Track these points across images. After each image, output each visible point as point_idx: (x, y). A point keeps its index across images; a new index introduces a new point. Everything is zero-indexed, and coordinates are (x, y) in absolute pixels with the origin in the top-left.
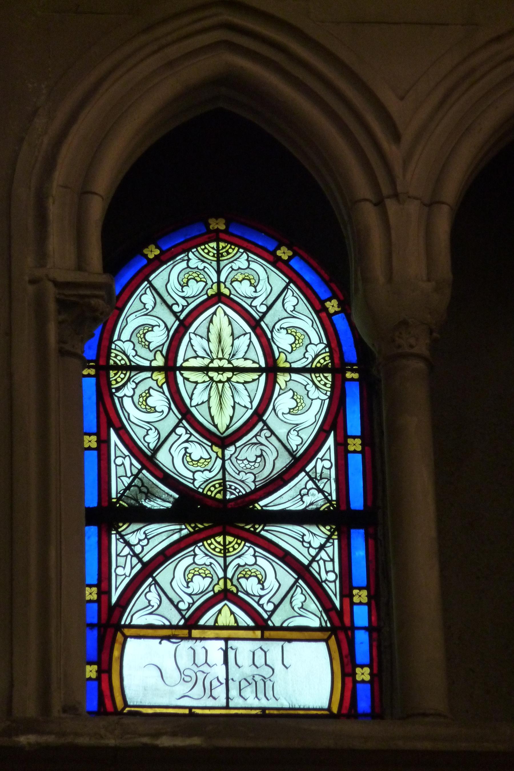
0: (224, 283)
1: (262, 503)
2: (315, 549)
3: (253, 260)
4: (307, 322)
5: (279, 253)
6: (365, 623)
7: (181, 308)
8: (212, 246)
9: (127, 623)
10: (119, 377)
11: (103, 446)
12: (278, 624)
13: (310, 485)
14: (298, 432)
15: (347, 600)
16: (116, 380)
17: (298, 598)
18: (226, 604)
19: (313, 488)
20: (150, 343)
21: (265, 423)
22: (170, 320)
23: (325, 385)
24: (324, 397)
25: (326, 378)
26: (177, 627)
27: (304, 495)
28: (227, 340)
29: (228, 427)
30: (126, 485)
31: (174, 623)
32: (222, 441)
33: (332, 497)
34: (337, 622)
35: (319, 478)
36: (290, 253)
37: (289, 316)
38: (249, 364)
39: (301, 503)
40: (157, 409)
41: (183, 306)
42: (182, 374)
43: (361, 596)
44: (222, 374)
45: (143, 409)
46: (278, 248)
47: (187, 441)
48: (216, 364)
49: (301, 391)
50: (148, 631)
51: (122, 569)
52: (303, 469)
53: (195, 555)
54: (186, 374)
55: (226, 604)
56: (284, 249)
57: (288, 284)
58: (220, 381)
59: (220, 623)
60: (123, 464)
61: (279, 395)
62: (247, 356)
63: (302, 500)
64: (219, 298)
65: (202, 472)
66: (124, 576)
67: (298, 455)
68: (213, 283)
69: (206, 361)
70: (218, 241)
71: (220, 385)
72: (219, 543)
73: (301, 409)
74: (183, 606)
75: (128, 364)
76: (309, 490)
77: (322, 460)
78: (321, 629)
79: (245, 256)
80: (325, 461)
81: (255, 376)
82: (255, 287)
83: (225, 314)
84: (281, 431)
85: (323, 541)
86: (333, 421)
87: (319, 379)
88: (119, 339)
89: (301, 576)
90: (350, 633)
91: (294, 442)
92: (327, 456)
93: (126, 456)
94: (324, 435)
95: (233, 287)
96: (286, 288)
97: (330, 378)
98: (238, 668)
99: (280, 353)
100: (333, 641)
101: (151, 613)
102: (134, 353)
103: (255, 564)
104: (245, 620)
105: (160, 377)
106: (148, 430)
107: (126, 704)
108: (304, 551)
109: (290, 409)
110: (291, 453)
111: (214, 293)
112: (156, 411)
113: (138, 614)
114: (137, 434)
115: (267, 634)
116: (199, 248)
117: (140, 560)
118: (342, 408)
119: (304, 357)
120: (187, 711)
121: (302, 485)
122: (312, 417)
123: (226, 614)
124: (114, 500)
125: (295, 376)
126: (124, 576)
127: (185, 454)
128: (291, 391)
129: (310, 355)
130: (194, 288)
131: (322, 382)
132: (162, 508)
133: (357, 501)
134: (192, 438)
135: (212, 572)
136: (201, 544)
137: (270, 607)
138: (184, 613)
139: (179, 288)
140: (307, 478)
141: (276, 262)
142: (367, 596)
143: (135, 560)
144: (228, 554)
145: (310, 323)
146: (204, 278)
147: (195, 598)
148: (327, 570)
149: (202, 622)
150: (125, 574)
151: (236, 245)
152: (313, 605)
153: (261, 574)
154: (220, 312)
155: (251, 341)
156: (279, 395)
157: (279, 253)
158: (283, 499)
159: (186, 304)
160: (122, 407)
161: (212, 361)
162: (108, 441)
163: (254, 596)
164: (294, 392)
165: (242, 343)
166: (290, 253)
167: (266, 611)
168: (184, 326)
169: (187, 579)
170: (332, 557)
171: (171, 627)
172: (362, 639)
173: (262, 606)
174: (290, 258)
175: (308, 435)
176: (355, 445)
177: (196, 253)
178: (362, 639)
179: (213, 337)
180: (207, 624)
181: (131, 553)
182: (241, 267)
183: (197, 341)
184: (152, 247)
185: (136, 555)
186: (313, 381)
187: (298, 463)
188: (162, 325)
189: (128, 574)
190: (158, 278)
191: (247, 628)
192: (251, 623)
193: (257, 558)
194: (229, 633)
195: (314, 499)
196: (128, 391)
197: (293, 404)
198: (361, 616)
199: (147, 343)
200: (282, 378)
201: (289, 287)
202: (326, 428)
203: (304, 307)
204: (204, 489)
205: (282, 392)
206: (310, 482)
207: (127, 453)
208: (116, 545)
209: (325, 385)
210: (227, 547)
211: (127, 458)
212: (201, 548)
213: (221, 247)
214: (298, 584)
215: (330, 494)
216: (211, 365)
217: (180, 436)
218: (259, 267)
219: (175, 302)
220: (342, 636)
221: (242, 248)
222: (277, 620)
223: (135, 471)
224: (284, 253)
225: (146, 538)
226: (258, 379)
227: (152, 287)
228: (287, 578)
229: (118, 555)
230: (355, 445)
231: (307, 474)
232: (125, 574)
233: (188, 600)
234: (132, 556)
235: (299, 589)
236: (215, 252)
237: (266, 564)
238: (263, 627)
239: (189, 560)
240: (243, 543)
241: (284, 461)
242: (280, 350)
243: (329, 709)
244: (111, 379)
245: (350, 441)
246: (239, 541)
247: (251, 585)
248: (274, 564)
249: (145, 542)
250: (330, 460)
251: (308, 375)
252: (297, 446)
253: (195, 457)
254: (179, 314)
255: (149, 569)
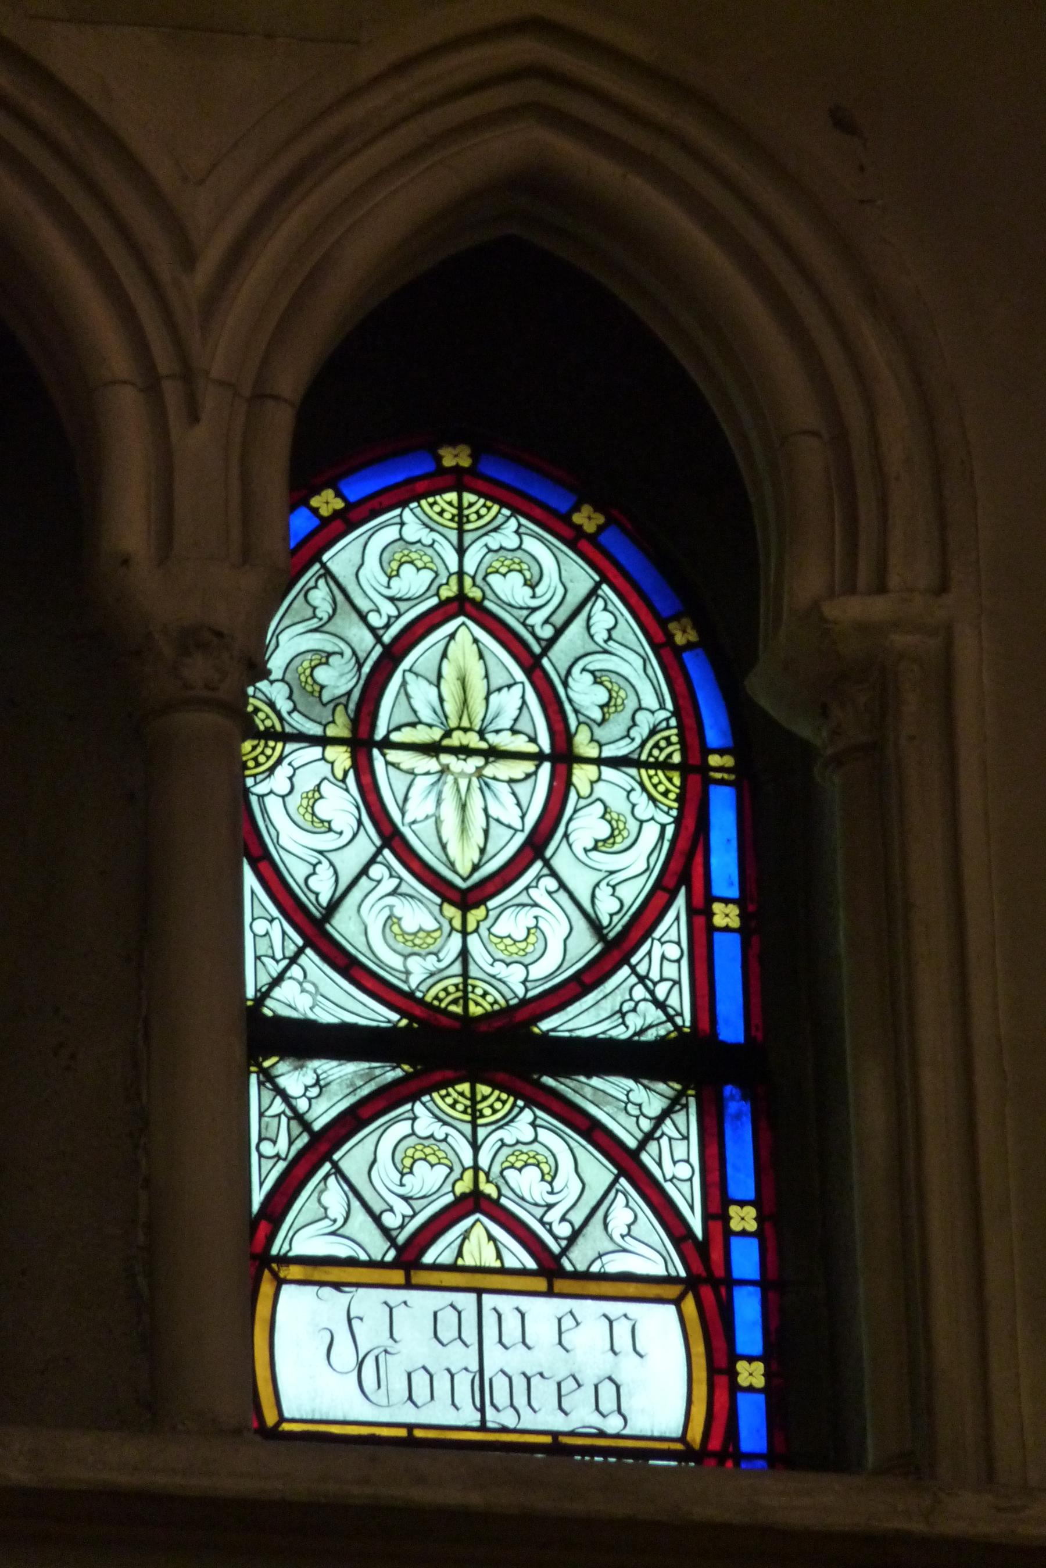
0: (452, 929)
1: (399, 1073)
2: (650, 1119)
3: (529, 532)
4: (633, 663)
5: (577, 518)
6: (754, 1274)
7: (384, 620)
8: (448, 500)
9: (283, 1252)
10: (262, 753)
11: (715, 1209)
12: (581, 1267)
13: (640, 992)
14: (614, 887)
15: (716, 1226)
16: (255, 759)
17: (619, 1216)
18: (478, 1220)
19: (645, 1000)
20: (322, 687)
21: (547, 863)
22: (562, 861)
23: (665, 794)
24: (667, 819)
25: (670, 780)
26: (381, 1265)
27: (313, 1086)
28: (477, 688)
29: (476, 868)
30: (668, 1122)
31: (378, 1257)
32: (467, 897)
33: (258, 1078)
34: (698, 1268)
35: (283, 1117)
36: (600, 519)
37: (599, 649)
38: (520, 744)
39: (319, 1071)
40: (334, 826)
41: (389, 617)
42: (384, 755)
43: (743, 1218)
44: (465, 760)
45: (302, 806)
46: (577, 509)
47: (394, 893)
48: (457, 739)
49: (618, 803)
50: (324, 1272)
51: (668, 955)
52: (625, 960)
53: (414, 1119)
54: (393, 755)
55: (465, 879)
56: (587, 509)
57: (597, 586)
58: (465, 730)
59: (468, 1260)
60: (675, 1163)
61: (575, 811)
62: (518, 727)
63: (624, 1023)
64: (461, 605)
65: (518, 1142)
66: (663, 940)
67: (612, 935)
68: (451, 575)
69: (436, 734)
70: (460, 489)
71: (465, 723)
72: (462, 1094)
73: (619, 836)
74: (391, 1221)
75: (278, 728)
76: (637, 1003)
77: (278, 1156)
78: (668, 1280)
79: (513, 524)
80: (667, 949)
81: (529, 766)
82: (533, 587)
83: (476, 641)
84: (581, 883)
85: (277, 993)
86: (682, 870)
87: (655, 780)
88: (663, 827)
89: (622, 1172)
90: (723, 1291)
91: (605, 907)
92: (267, 1164)
93: (671, 1180)
94: (662, 897)
95: (489, 584)
96: (593, 594)
97: (677, 781)
98: (506, 1370)
99: (580, 723)
100: (689, 1304)
101: (612, 873)
102: (289, 705)
103: (535, 1140)
104: (518, 1257)
105: (341, 756)
106: (629, 1234)
107: (282, 1419)
108: (630, 1123)
109: (597, 841)
110: (596, 926)
111: (451, 594)
112: (330, 830)
113: (303, 1236)
114: (295, 870)
115: (560, 1285)
116: (423, 502)
117: (306, 1126)
118: (701, 840)
119: (628, 736)
120: (402, 1433)
121: (622, 994)
122: (637, 866)
123: (479, 1243)
124: (691, 1092)
125: (608, 772)
126: (663, 940)
127: (554, 1178)
128: (599, 803)
129: (640, 733)
130: (412, 581)
131: (661, 788)
132: (646, 1082)
133: (731, 1028)
134: (539, 1212)
135: (451, 1155)
136: (512, 1002)
137: (564, 1230)
138: (545, 871)
139: (384, 580)
140: (634, 979)
141: (574, 540)
142: (755, 1219)
143: (296, 1129)
144: (480, 1121)
145: (639, 662)
146: (432, 562)
147: (524, 899)
148: (676, 1158)
149: (428, 1258)
150: (662, 944)
151: (495, 501)
152: (649, 1227)
153: (547, 1163)
154: (463, 635)
155: (524, 702)
156: (575, 811)
157: (577, 518)
158: (342, 1081)
159: (395, 613)
160: (264, 810)
161: (448, 734)
162: (707, 1217)
163: (536, 1205)
164: (606, 807)
165: (507, 703)
166: (600, 519)
167: (556, 1238)
168: (392, 655)
169: (412, 1158)
170: (259, 963)
171: (371, 1264)
172: (748, 1307)
173: (549, 1227)
174: (600, 529)
175: (634, 893)
176: (725, 916)
177: (418, 511)
178: (748, 1307)
179: (450, 687)
180: (440, 1261)
181: (289, 1113)
182: (504, 545)
183: (512, 816)
184: (329, 494)
185: (642, 979)
186: (642, 784)
187: (617, 948)
188: (348, 652)
189: (283, 1156)
190: (340, 557)
191: (523, 1272)
192: (531, 1264)
193: (538, 1129)
194: (480, 1281)
195: (645, 1022)
196: (279, 781)
197: (604, 831)
198: (746, 1260)
199: (317, 688)
200: (582, 775)
201: (600, 592)
202: (670, 882)
203: (629, 630)
204: (514, 1105)
205: (582, 803)
206: (640, 987)
207: (669, 1187)
208: (681, 1001)
209: (665, 794)
210: (479, 1106)
211: (668, 1177)
212: (512, 995)
213: (465, 504)
214: (618, 1186)
215: (681, 1014)
216: (446, 742)
217: (563, 1219)
218: (541, 549)
219: (374, 607)
220: (707, 1291)
221: (508, 507)
222: (579, 1259)
223: (652, 1147)
224: (587, 519)
225: (623, 1015)
226: (535, 773)
227: (327, 573)
228: (599, 1172)
229: (261, 1115)
230: (725, 916)
231: (633, 968)
232: (662, 944)
233: (538, 894)
234: (289, 1119)
235: (620, 1196)
236: (455, 511)
237: (385, 957)
238: (552, 1274)
239: (403, 1128)
240: (512, 1099)
241: (585, 946)
242: (582, 718)
243: (682, 1439)
244: (244, 758)
245: (717, 907)
246: (504, 1096)
247: (527, 1183)
248: (573, 1144)
249: (626, 1007)
250: (679, 943)
251: (633, 771)
252: (611, 915)
253: (532, 1173)
254: (381, 632)
255: (321, 1147)
